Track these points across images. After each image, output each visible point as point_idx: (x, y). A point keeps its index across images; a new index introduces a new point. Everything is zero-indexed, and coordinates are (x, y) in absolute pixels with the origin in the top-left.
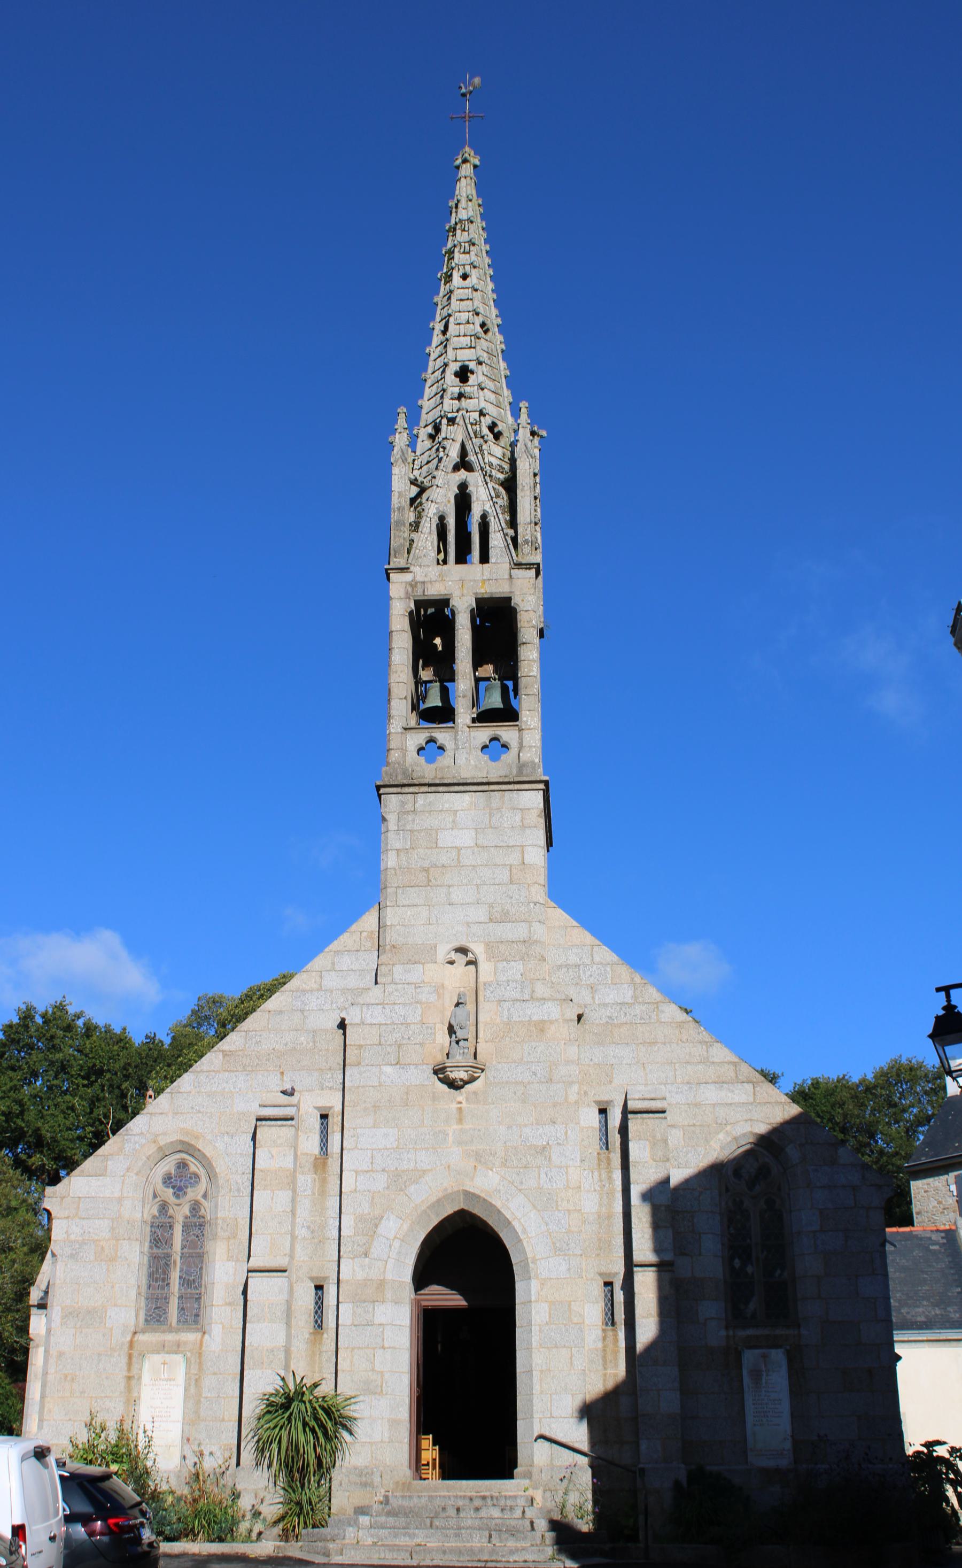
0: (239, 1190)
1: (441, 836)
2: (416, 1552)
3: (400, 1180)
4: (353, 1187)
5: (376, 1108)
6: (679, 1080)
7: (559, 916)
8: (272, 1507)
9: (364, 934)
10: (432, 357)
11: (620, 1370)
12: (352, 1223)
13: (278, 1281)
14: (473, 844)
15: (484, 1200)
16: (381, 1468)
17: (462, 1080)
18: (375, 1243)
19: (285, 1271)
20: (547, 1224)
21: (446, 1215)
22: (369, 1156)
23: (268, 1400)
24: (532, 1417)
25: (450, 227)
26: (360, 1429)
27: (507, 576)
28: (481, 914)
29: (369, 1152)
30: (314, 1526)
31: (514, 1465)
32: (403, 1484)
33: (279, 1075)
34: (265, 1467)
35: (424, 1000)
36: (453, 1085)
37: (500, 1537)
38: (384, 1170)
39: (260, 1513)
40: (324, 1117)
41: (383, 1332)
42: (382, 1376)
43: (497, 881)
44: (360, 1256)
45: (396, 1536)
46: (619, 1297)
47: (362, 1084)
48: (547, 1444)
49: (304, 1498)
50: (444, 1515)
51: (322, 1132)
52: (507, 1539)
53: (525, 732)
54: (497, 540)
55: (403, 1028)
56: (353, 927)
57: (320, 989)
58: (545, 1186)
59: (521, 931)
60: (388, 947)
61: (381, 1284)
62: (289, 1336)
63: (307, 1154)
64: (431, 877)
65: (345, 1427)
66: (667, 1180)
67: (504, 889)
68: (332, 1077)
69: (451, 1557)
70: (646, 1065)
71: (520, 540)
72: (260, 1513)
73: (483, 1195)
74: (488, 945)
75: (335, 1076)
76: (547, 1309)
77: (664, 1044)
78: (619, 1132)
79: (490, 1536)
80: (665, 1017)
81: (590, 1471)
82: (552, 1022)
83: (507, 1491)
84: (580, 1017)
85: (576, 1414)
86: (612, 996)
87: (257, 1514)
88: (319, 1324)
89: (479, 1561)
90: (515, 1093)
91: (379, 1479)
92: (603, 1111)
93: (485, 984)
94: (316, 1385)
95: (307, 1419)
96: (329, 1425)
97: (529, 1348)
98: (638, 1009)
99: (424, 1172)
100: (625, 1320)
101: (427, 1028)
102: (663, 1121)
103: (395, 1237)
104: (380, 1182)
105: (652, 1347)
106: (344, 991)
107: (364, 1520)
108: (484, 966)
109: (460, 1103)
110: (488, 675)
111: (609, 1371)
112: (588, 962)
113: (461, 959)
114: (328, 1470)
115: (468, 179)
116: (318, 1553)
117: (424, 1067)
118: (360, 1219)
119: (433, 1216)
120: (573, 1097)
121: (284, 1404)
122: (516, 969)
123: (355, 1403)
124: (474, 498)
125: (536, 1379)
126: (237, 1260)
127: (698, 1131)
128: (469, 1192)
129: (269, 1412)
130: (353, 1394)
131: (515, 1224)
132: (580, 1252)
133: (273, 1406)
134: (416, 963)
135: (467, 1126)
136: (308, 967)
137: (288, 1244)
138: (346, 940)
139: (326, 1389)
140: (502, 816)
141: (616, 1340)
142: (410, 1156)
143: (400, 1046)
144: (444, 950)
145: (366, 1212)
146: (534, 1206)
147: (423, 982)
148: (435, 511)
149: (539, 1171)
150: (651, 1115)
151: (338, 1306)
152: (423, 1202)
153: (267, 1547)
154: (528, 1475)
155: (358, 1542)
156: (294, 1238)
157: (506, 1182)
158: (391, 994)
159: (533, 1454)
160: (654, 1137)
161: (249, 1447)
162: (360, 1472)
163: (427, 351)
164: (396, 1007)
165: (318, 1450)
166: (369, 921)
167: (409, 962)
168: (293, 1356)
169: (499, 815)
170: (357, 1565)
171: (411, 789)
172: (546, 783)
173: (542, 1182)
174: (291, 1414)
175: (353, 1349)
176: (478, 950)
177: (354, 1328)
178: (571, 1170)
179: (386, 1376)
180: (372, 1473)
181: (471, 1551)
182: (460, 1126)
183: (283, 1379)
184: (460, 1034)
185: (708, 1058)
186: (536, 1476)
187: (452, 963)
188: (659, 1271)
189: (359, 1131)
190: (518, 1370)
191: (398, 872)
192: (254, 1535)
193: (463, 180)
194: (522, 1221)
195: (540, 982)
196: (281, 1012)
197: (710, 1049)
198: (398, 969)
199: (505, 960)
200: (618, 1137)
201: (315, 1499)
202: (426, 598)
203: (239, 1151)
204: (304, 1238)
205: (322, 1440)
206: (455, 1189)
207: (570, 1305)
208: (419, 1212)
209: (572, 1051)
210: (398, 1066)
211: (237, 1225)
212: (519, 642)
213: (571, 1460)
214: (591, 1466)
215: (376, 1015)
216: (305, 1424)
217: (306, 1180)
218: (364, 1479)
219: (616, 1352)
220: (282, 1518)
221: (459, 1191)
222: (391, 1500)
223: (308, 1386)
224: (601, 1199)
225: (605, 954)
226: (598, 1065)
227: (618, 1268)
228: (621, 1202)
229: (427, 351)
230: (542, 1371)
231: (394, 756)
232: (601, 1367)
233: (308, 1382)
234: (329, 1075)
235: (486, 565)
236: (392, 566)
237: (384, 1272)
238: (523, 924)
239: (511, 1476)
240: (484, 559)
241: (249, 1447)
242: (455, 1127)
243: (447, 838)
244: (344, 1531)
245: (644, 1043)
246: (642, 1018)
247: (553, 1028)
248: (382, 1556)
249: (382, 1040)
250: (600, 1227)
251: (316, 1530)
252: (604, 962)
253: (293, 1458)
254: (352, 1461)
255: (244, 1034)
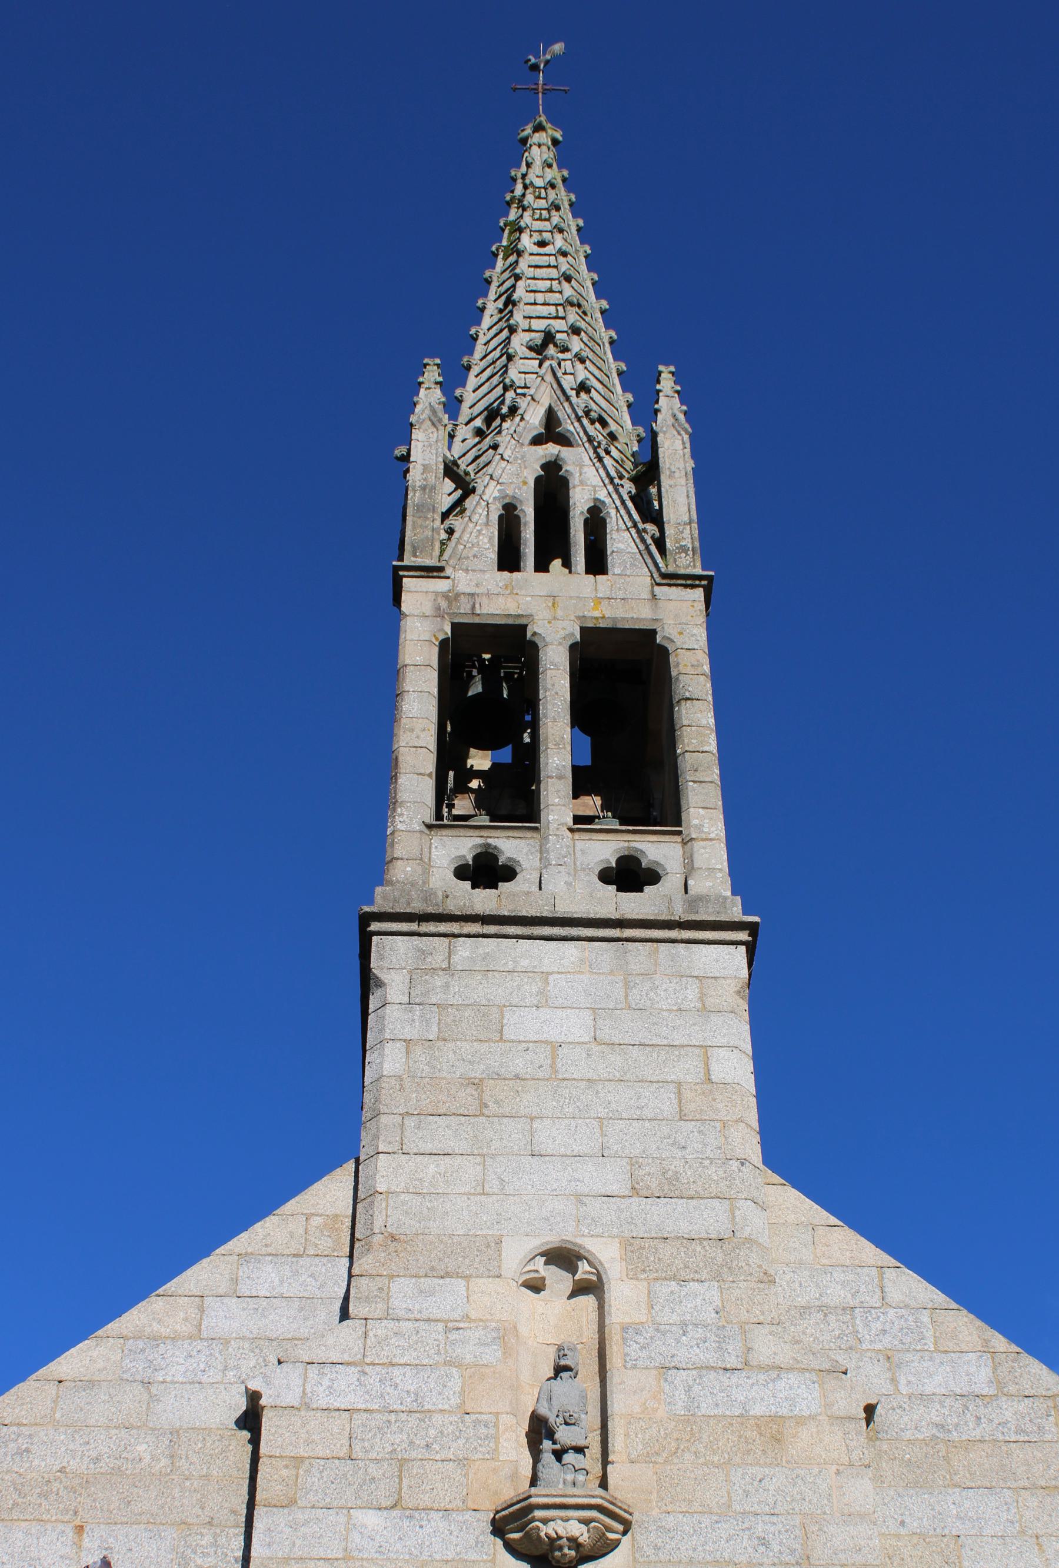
1: (511, 1018)
7: (793, 1204)
9: (317, 1221)
10: (482, 340)
14: (586, 1039)
17: (573, 1541)
25: (513, 198)
27: (646, 595)
28: (612, 1177)
43: (647, 1113)
53: (697, 845)
54: (621, 542)
56: (290, 1206)
57: (197, 1335)
59: (710, 1218)
60: (377, 1239)
64: (486, 1098)
67: (666, 1130)
68: (215, 1544)
71: (669, 544)
74: (631, 1245)
75: (222, 1540)
82: (801, 1421)
84: (870, 1410)
86: (938, 1379)
93: (625, 1329)
101: (477, 1422)
106: (257, 1341)
108: (623, 1295)
110: (591, 813)
112: (875, 1301)
113: (559, 1280)
115: (544, 148)
117: (468, 1516)
122: (702, 1299)
124: (574, 481)
134: (447, 1275)
136: (171, 1286)
138: (270, 1231)
140: (654, 988)
143: (402, 1463)
144: (518, 1253)
147: (467, 1317)
148: (496, 494)
163: (473, 331)
164: (396, 1371)
166: (332, 1192)
169: (647, 985)
171: (443, 927)
172: (753, 928)
176: (605, 1253)
184: (565, 1435)
187: (535, 1286)
191: (407, 1083)
193: (535, 149)
195: (765, 1330)
196: (92, 1383)
198: (403, 1293)
199: (674, 1278)
202: (477, 620)
210: (396, 1513)
212: (676, 698)
215: (343, 1389)
225: (909, 1286)
229: (473, 331)
231: (402, 871)
234: (207, 1540)
235: (600, 578)
236: (406, 563)
238: (716, 1203)
240: (597, 564)
243: (523, 1024)
245: (1033, 1488)
246: (1019, 1431)
249: (357, 1448)
252: (913, 1304)
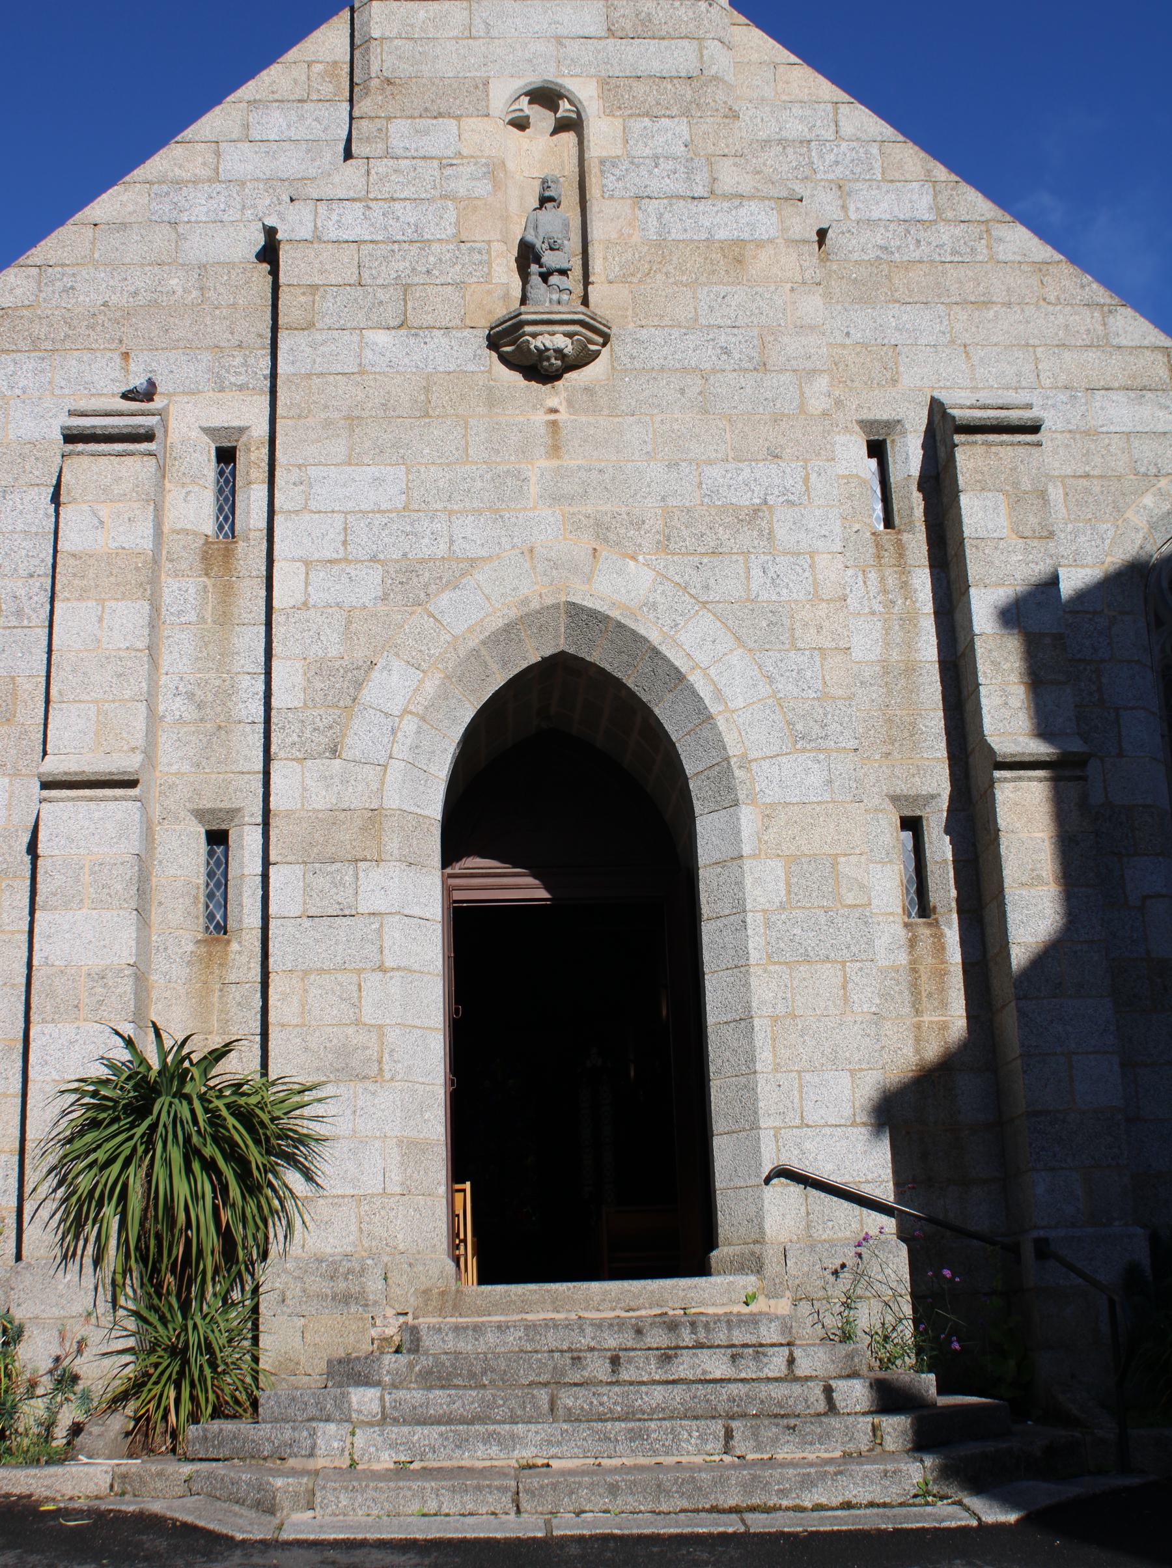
0: (19, 613)
2: (531, 1492)
3: (413, 582)
4: (300, 598)
5: (353, 421)
6: (1047, 383)
8: (107, 1362)
9: (318, 68)
11: (952, 1018)
12: (299, 679)
13: (115, 809)
15: (620, 625)
16: (386, 1259)
17: (559, 352)
18: (356, 724)
19: (133, 784)
20: (770, 679)
21: (525, 665)
22: (339, 525)
23: (95, 1094)
24: (754, 1126)
26: (330, 1164)
29: (340, 518)
30: (217, 1414)
31: (708, 1238)
32: (443, 1293)
33: (118, 359)
34: (88, 1261)
35: (462, 192)
36: (539, 369)
37: (755, 1435)
38: (374, 559)
39: (75, 1378)
40: (226, 456)
41: (380, 931)
42: (382, 1036)
44: (320, 755)
45: (461, 1443)
46: (940, 849)
47: (318, 369)
48: (795, 1189)
49: (193, 1339)
50: (577, 1378)
51: (220, 491)
52: (775, 1441)
55: (414, 249)
56: (293, 54)
57: (215, 178)
58: (764, 596)
59: (679, 57)
60: (375, 83)
61: (375, 818)
62: (143, 944)
63: (187, 532)
65: (291, 1160)
66: (1053, 582)
69: (632, 1502)
70: (970, 349)
72: (75, 1378)
73: (615, 614)
74: (607, 84)
75: (251, 361)
76: (780, 872)
77: (1009, 305)
78: (921, 488)
79: (729, 1435)
80: (1004, 252)
81: (904, 1248)
82: (760, 244)
83: (703, 1303)
84: (822, 234)
85: (862, 1117)
87: (66, 1380)
88: (218, 927)
89: (714, 1509)
90: (682, 391)
91: (380, 1284)
92: (877, 449)
93: (602, 162)
94: (218, 1055)
95: (195, 1139)
96: (255, 1156)
97: (741, 967)
98: (946, 234)
99: (473, 562)
100: (959, 901)
101: (472, 250)
102: (1034, 450)
103: (406, 711)
104: (368, 585)
105: (1048, 957)
107: (364, 1399)
108: (601, 131)
109: (556, 411)
111: (926, 1018)
112: (829, 134)
113: (542, 119)
114: (250, 1264)
116: (239, 1502)
117: (467, 333)
118: (319, 668)
119: (494, 667)
120: (817, 403)
121: (137, 1103)
122: (672, 134)
123: (319, 1100)
125: (761, 1036)
126: (16, 774)
127: (1097, 489)
128: (583, 609)
129: (95, 1124)
130: (308, 1080)
131: (696, 679)
132: (853, 744)
133: (104, 1108)
134: (440, 115)
135: (571, 461)
136: (188, 133)
137: (140, 724)
138: (275, 78)
139: (240, 1065)
141: (940, 948)
142: (437, 526)
143: (406, 287)
144: (504, 93)
145: (333, 652)
146: (738, 639)
147: (459, 154)
149: (747, 561)
150: (1005, 437)
151: (265, 877)
152: (471, 630)
153: (85, 1481)
154: (753, 1264)
155: (353, 1464)
156: (153, 719)
157: (668, 586)
158: (382, 179)
159: (757, 1211)
160: (1016, 485)
161: (44, 1213)
162: (333, 1269)
164: (397, 205)
165: (226, 1216)
167: (425, 113)
168: (154, 995)
170: (363, 1544)
173: (754, 586)
174: (153, 1127)
175: (306, 973)
176: (584, 91)
177: (307, 923)
178: (822, 561)
179: (392, 1036)
180: (363, 1271)
181: (687, 1478)
182: (555, 463)
183: (129, 1043)
184: (550, 259)
185: (1106, 336)
186: (772, 1266)
187: (521, 124)
188: (1056, 780)
189: (313, 471)
190: (711, 1019)
192: (60, 1433)
194: (712, 672)
195: (729, 162)
196: (124, 226)
197: (1111, 320)
198: (399, 129)
199: (647, 114)
200: (917, 499)
201: (219, 1340)
203: (20, 526)
204: (181, 721)
205: (235, 1191)
206: (549, 601)
207: (835, 865)
208: (462, 653)
209: (812, 306)
210: (403, 332)
211: (14, 694)
213: (855, 1226)
214: (903, 1235)
215: (350, 222)
216: (191, 1153)
217: (183, 591)
218: (342, 1285)
219: (941, 974)
220: (136, 1387)
221: (556, 606)
222: (427, 1341)
223: (195, 1058)
224: (887, 631)
225: (861, 121)
226: (865, 345)
227: (936, 782)
228: (934, 640)
230: (775, 1019)
232: (907, 1010)
233: (199, 1049)
234: (238, 360)
237: (381, 790)
238: (685, 42)
239: (702, 1269)
241: (44, 1213)
242: (544, 463)
244: (313, 1434)
246: (954, 252)
247: (764, 256)
248: (432, 1506)
249: (366, 274)
250: (889, 693)
251: (229, 1426)
252: (864, 137)
253: (158, 1237)
254: (310, 1242)
255: (34, 271)
